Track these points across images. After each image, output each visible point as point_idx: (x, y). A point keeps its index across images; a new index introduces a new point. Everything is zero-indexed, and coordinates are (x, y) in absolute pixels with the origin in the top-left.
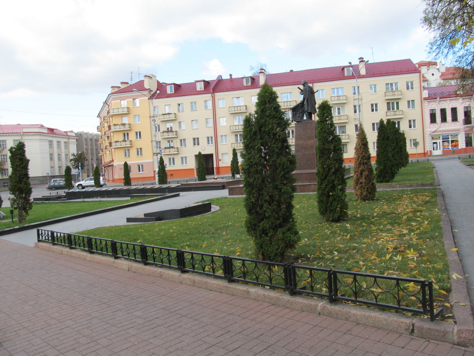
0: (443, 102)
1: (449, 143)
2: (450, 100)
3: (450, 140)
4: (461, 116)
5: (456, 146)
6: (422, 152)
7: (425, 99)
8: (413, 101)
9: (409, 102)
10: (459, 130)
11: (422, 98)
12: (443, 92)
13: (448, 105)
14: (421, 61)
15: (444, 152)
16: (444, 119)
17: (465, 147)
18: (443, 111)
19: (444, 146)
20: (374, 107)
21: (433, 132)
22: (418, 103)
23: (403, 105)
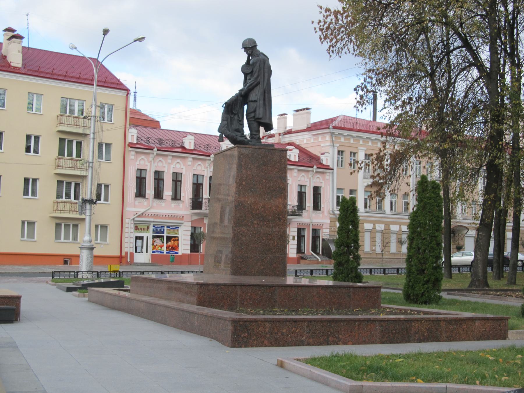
1: (163, 242)
3: (165, 235)
4: (187, 193)
5: (175, 248)
6: (118, 254)
7: (132, 146)
8: (108, 145)
10: (182, 218)
11: (127, 143)
13: (169, 166)
15: (153, 257)
16: (158, 194)
17: (189, 252)
18: (159, 177)
19: (155, 246)
20: (32, 144)
21: (139, 216)
22: (117, 150)
23: (89, 150)
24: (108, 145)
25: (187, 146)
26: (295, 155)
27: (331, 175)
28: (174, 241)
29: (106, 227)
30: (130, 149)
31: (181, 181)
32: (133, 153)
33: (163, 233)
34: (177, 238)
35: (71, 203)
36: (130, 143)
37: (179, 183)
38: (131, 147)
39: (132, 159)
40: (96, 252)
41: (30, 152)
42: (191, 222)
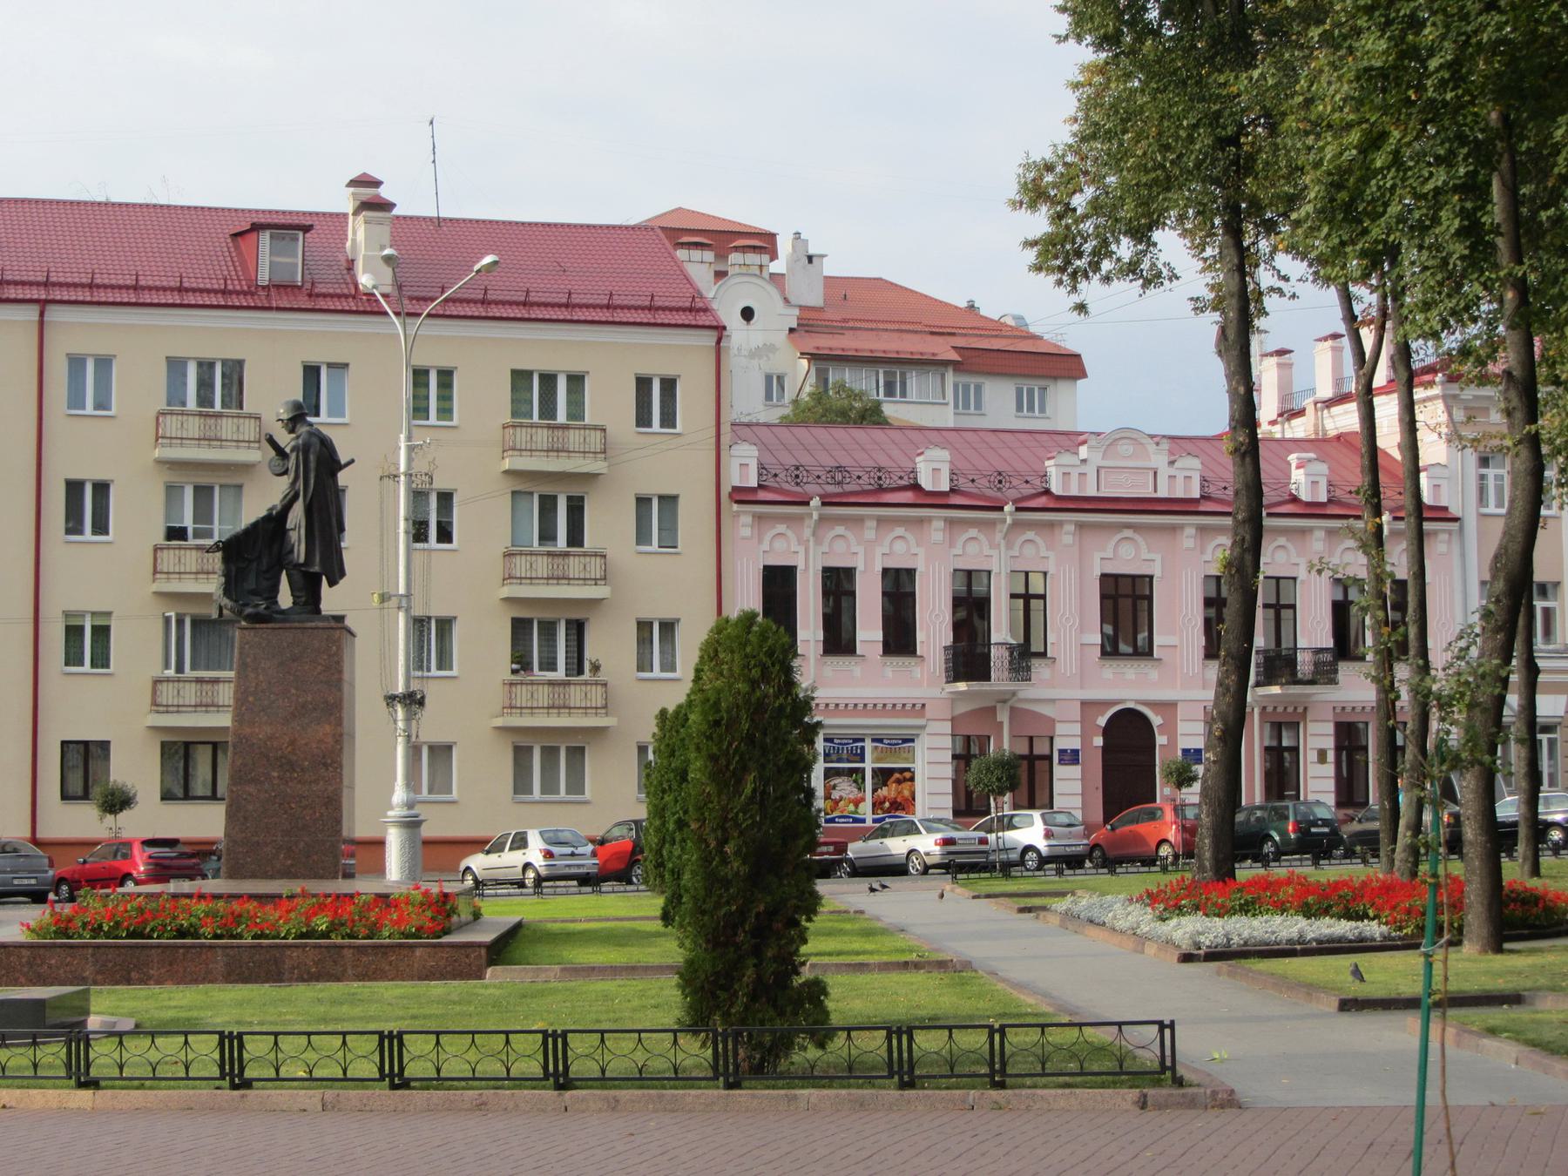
0: (840, 530)
2: (880, 520)
3: (868, 766)
4: (934, 625)
7: (742, 496)
8: (669, 501)
9: (643, 502)
10: (919, 709)
12: (839, 468)
13: (868, 551)
14: (679, 211)
19: (836, 802)
22: (694, 518)
23: (609, 524)
24: (669, 501)
25: (926, 483)
26: (1188, 478)
27: (1455, 538)
28: (899, 782)
29: (448, 748)
30: (735, 507)
31: (1293, 607)
32: (747, 519)
33: (863, 761)
34: (907, 775)
35: (586, 683)
36: (736, 489)
37: (1286, 614)
38: (738, 502)
39: (744, 538)
40: (427, 831)
41: (426, 540)
42: (953, 720)
